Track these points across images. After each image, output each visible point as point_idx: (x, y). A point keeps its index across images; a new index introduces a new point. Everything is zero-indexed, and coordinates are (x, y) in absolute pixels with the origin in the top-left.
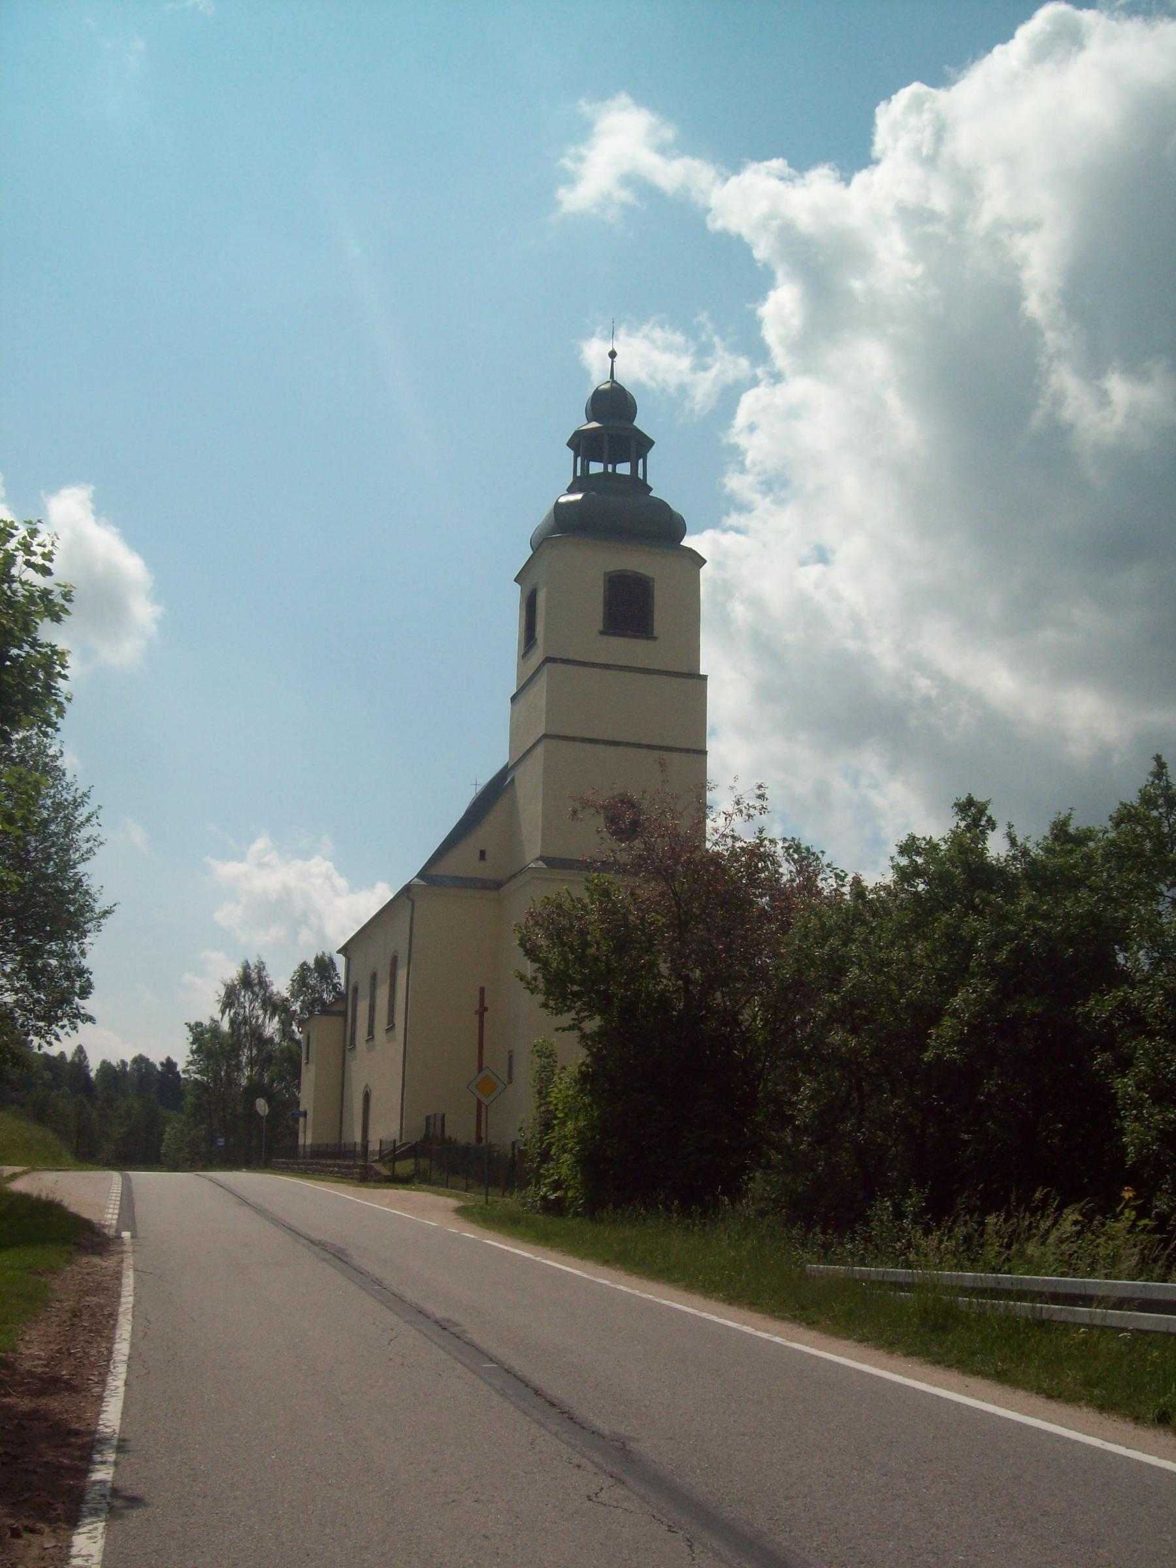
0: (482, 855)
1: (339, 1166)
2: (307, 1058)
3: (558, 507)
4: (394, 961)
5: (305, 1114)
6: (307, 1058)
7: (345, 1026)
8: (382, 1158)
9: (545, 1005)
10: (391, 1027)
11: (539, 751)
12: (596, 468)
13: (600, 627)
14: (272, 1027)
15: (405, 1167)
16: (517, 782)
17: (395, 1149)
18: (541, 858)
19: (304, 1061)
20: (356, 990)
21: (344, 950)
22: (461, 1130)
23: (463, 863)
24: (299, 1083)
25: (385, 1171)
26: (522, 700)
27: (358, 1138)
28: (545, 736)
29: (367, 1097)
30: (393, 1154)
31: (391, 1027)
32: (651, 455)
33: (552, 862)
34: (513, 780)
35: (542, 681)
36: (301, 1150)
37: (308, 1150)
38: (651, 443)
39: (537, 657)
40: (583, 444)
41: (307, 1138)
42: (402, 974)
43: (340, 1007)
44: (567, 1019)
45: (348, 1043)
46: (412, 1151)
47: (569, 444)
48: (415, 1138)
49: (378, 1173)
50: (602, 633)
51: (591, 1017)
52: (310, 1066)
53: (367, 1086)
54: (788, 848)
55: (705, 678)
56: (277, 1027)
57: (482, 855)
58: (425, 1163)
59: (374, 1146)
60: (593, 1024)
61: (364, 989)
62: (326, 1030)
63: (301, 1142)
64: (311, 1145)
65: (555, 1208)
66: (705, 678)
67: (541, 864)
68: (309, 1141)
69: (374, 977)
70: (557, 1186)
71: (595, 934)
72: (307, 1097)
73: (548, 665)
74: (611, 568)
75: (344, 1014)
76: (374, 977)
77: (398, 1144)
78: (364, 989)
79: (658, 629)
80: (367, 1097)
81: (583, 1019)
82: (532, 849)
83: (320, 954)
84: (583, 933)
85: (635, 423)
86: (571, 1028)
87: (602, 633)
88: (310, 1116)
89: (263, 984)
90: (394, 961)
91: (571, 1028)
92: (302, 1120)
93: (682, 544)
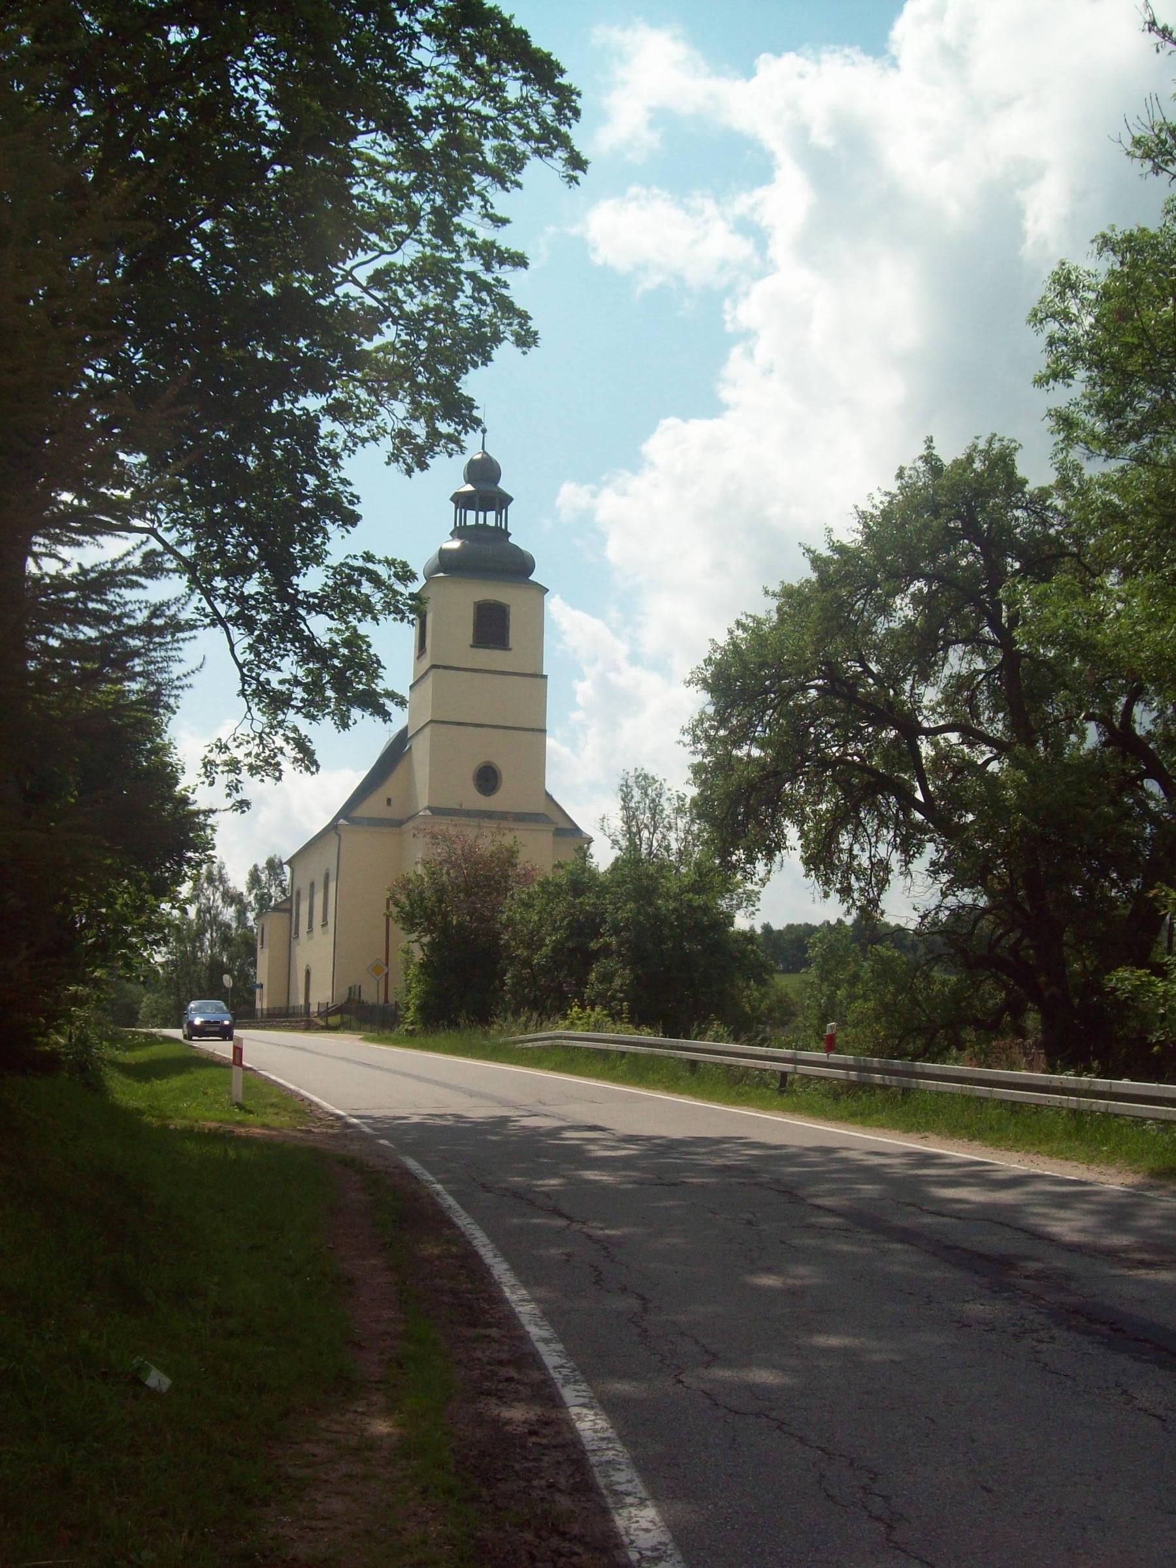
0: (389, 801)
1: (290, 1022)
2: (262, 944)
3: (442, 552)
4: (327, 876)
5: (261, 986)
6: (262, 944)
7: (291, 922)
8: (319, 1014)
9: (403, 929)
10: (325, 924)
11: (427, 731)
12: (471, 518)
13: (471, 642)
14: (229, 914)
15: (334, 1020)
16: (413, 750)
17: (328, 1009)
18: (429, 808)
19: (259, 946)
20: (298, 893)
21: (289, 862)
22: (370, 995)
23: (373, 807)
24: (255, 962)
25: (322, 1023)
26: (416, 688)
27: (302, 1001)
28: (431, 721)
29: (308, 973)
30: (326, 1012)
31: (325, 924)
32: (511, 507)
33: (436, 811)
34: (410, 748)
35: (428, 683)
36: (259, 1015)
37: (265, 1012)
38: (511, 499)
39: (427, 662)
40: (462, 501)
41: (262, 1003)
42: (332, 886)
43: (287, 906)
44: (414, 936)
45: (293, 934)
46: (339, 1010)
47: (452, 499)
48: (341, 1001)
49: (317, 1024)
50: (472, 646)
51: (425, 936)
52: (264, 950)
53: (308, 966)
54: (638, 777)
55: (546, 677)
56: (233, 914)
57: (389, 801)
58: (347, 1017)
59: (314, 1008)
60: (426, 939)
61: (305, 893)
62: (275, 924)
63: (258, 1006)
64: (268, 1009)
65: (411, 1033)
66: (546, 677)
67: (428, 813)
68: (265, 1006)
69: (312, 885)
70: (412, 1023)
71: (427, 894)
72: (262, 974)
73: (434, 670)
74: (479, 598)
75: (290, 911)
76: (312, 885)
77: (330, 1005)
78: (305, 893)
79: (512, 642)
80: (308, 973)
81: (421, 937)
82: (423, 800)
83: (272, 855)
84: (421, 893)
85: (500, 485)
86: (416, 941)
87: (472, 646)
88: (265, 987)
89: (222, 880)
90: (327, 876)
91: (416, 941)
92: (258, 991)
93: (530, 578)
